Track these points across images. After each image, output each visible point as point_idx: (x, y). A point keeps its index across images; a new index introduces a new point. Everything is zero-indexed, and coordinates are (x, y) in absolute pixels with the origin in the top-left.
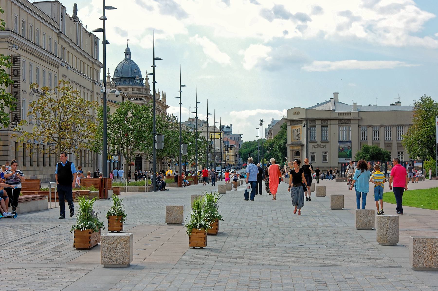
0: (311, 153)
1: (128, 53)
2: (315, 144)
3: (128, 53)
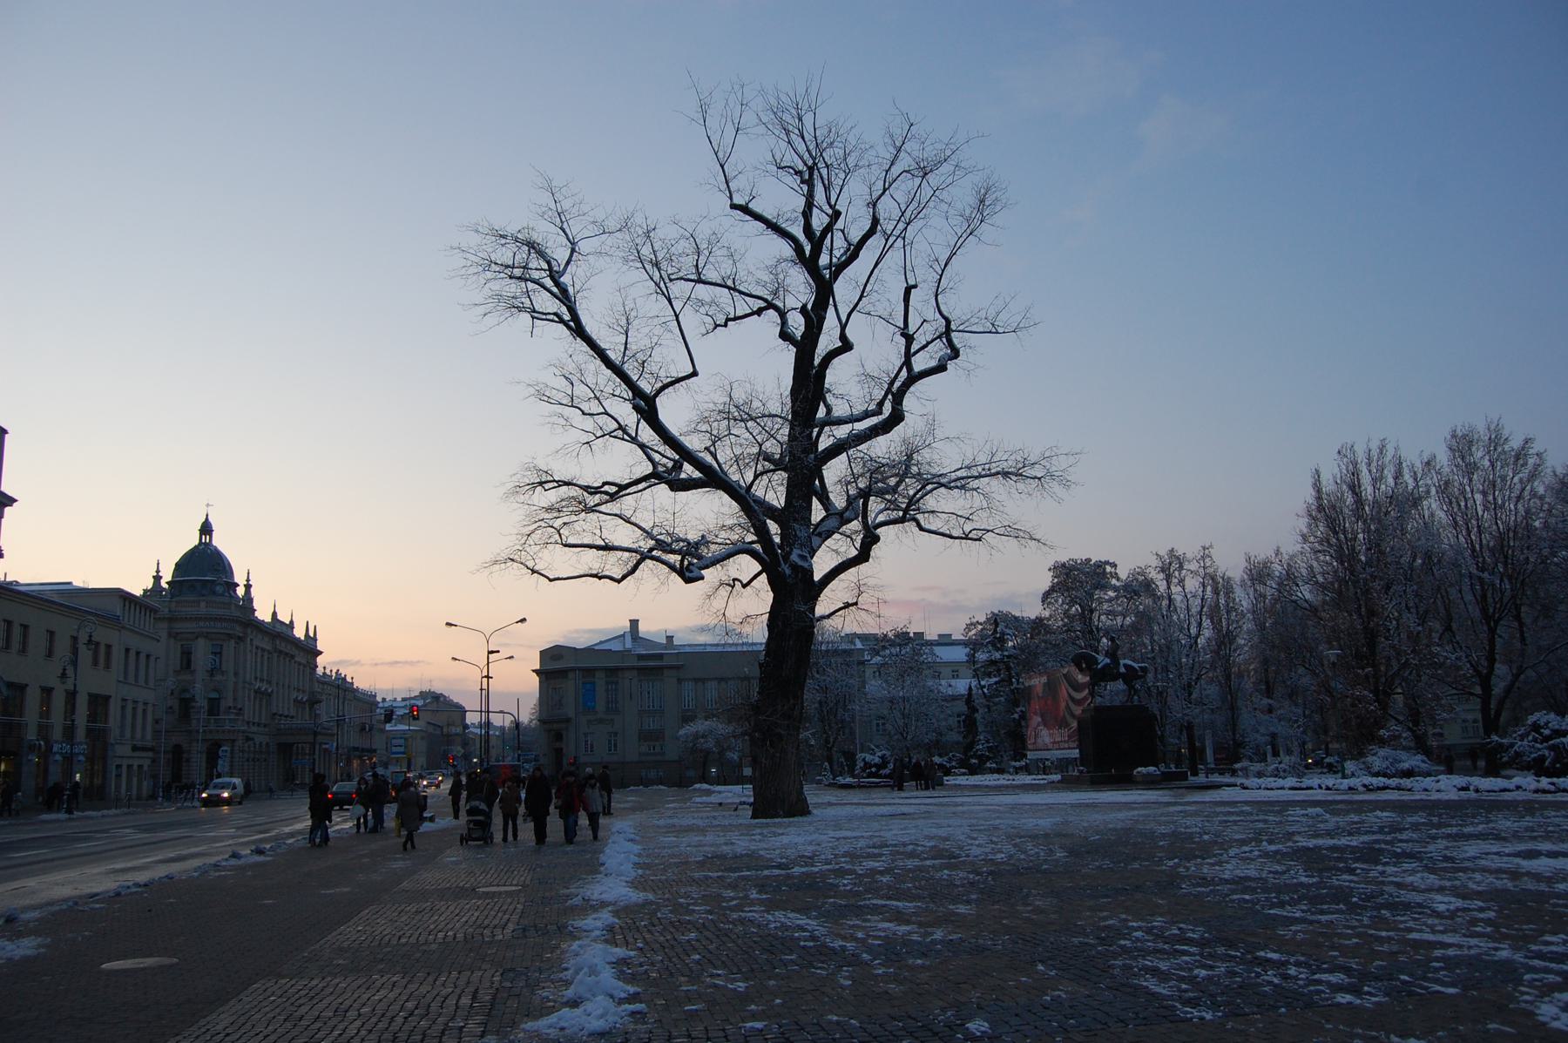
1: (206, 529)
3: (206, 529)
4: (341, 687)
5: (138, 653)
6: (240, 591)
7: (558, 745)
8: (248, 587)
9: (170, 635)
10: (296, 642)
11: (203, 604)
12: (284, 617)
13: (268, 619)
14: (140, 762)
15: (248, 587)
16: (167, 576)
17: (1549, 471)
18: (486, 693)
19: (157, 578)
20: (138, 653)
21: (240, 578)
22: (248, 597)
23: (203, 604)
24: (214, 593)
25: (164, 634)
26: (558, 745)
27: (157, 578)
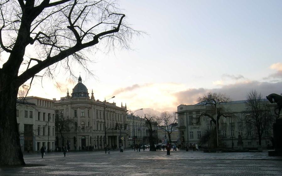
0: (191, 132)
2: (193, 127)
3: (80, 79)
4: (132, 117)
5: (44, 113)
6: (90, 95)
7: (183, 135)
8: (92, 94)
9: (71, 108)
10: (118, 108)
11: (78, 99)
12: (124, 105)
13: (120, 107)
14: (101, 135)
15: (92, 94)
16: (71, 92)
17: (272, 79)
18: (205, 95)
19: (68, 93)
20: (44, 113)
21: (90, 92)
22: (93, 97)
23: (78, 99)
24: (81, 96)
25: (70, 108)
26: (183, 135)
27: (68, 93)
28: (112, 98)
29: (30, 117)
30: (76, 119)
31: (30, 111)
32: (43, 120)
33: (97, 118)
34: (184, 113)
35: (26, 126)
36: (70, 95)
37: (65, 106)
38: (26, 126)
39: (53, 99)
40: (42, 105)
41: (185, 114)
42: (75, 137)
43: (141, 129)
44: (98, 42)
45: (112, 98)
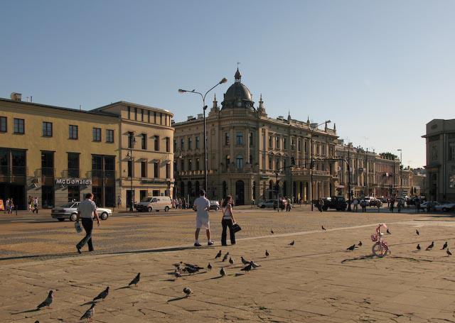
3: (238, 76)
6: (256, 106)
8: (261, 102)
15: (261, 102)
16: (220, 99)
19: (215, 102)
22: (261, 110)
25: (217, 129)
27: (215, 102)
28: (221, 83)
29: (108, 142)
30: (228, 149)
31: (44, 122)
32: (140, 148)
33: (270, 148)
34: (439, 135)
35: (97, 159)
36: (220, 106)
37: (210, 125)
38: (97, 159)
39: (199, 115)
40: (164, 123)
41: (441, 137)
42: (224, 182)
43: (364, 169)
44: (427, 125)
45: (221, 83)
